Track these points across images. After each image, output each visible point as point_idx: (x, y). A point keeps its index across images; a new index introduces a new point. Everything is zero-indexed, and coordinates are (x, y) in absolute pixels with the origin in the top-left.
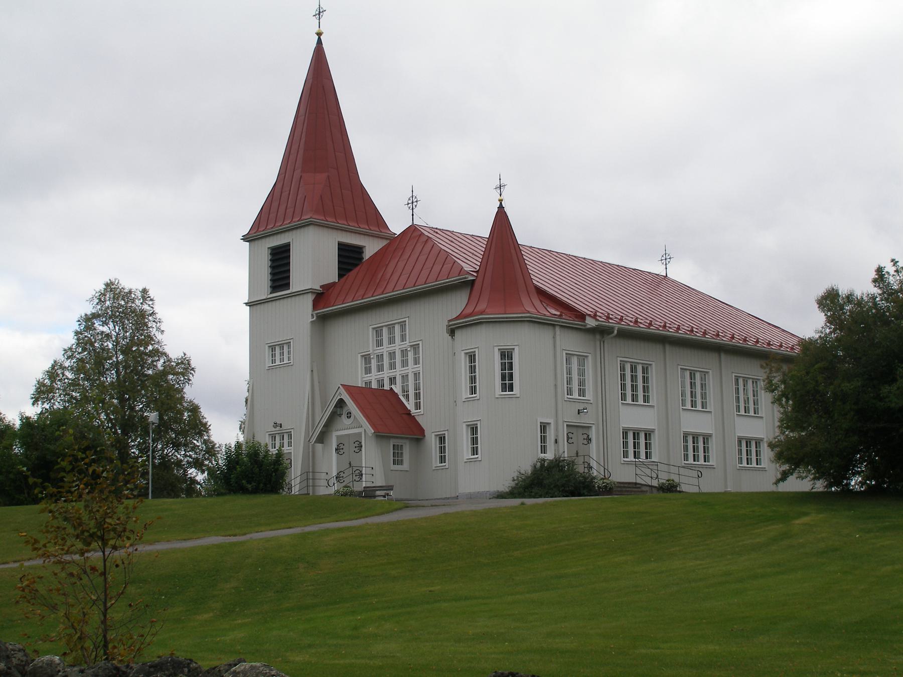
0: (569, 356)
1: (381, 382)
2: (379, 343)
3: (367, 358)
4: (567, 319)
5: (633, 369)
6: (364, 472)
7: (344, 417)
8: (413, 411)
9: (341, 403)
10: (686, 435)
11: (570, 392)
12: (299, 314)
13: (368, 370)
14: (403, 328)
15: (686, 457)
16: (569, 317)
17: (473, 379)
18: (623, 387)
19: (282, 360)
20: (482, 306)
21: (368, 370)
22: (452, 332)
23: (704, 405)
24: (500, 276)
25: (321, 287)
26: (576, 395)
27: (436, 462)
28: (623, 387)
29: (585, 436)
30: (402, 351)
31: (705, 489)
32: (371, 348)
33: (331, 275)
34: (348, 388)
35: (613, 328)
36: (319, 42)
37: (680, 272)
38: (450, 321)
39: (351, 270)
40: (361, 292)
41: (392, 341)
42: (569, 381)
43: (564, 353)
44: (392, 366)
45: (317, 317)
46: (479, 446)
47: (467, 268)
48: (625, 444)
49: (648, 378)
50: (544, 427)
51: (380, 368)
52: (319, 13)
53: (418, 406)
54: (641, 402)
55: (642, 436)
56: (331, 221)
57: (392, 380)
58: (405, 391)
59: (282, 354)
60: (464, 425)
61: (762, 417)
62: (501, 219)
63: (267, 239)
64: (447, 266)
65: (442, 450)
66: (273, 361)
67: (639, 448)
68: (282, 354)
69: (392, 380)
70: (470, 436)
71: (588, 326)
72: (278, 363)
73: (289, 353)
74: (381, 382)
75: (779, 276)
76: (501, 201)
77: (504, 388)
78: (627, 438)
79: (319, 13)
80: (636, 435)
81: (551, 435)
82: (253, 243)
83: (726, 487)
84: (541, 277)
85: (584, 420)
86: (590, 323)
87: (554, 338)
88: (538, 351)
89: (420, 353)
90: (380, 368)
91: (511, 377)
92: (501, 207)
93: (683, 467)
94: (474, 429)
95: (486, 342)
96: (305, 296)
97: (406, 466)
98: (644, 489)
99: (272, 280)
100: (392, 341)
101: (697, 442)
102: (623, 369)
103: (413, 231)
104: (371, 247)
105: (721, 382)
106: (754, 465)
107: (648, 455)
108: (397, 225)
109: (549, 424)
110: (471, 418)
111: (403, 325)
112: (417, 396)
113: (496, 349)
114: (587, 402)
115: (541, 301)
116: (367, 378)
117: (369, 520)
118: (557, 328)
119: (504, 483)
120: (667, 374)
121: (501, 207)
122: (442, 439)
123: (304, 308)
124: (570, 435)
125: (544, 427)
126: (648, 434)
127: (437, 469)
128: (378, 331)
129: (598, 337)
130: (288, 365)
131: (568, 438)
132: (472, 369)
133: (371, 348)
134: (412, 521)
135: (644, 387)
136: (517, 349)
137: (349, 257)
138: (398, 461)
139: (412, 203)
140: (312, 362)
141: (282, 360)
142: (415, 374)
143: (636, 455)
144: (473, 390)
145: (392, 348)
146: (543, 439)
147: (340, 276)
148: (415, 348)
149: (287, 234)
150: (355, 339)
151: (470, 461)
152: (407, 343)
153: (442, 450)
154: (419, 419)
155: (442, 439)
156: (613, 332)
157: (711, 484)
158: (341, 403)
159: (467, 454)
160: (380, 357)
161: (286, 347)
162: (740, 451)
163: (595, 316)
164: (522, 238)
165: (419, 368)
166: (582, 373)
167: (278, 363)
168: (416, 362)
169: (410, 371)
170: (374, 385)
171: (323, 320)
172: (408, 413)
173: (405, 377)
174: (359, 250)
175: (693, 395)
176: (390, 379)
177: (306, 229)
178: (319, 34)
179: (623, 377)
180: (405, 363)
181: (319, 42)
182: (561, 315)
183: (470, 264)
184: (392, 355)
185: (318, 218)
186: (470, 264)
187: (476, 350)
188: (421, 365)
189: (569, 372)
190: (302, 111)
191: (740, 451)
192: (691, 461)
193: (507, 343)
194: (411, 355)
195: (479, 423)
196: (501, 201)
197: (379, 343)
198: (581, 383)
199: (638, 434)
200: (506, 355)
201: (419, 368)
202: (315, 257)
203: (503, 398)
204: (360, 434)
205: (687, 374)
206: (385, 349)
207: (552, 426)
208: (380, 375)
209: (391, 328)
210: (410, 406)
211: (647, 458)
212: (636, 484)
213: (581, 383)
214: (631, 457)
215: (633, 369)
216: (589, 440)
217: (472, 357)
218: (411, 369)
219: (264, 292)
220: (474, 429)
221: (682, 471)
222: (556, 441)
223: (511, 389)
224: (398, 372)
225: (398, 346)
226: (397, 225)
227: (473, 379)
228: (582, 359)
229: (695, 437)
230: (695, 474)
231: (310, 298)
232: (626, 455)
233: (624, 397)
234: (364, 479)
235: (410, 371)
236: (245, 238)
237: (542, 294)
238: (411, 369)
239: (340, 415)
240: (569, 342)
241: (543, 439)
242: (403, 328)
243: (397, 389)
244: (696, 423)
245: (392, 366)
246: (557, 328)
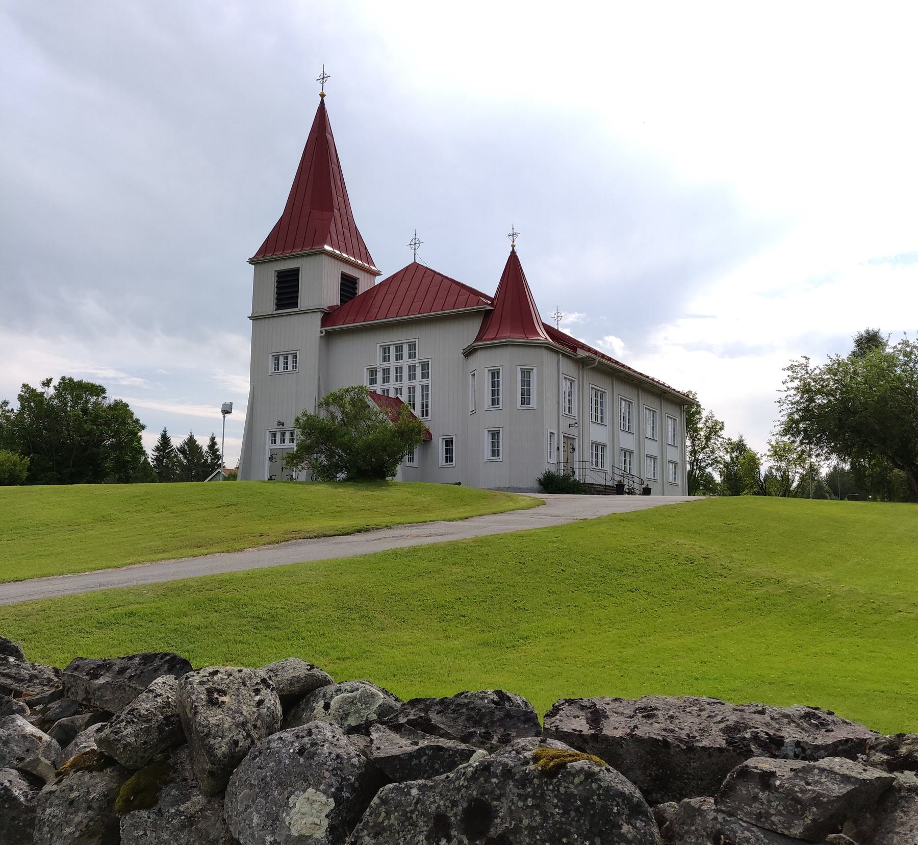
2: (386, 359)
12: (304, 332)
32: (379, 363)
36: (322, 103)
52: (323, 78)
53: (425, 413)
58: (412, 399)
60: (486, 431)
66: (277, 369)
69: (399, 391)
76: (513, 246)
79: (323, 78)
82: (259, 266)
86: (581, 353)
94: (495, 435)
97: (415, 463)
111: (412, 346)
112: (425, 406)
122: (449, 442)
126: (604, 447)
128: (386, 350)
133: (379, 363)
134: (519, 536)
136: (535, 369)
137: (348, 284)
139: (415, 244)
148: (425, 365)
160: (386, 371)
165: (428, 382)
171: (329, 337)
173: (412, 390)
178: (323, 96)
181: (322, 103)
184: (399, 370)
194: (418, 371)
197: (386, 359)
201: (428, 382)
206: (392, 364)
210: (417, 412)
216: (574, 449)
219: (269, 306)
220: (495, 435)
225: (405, 362)
231: (319, 316)
236: (252, 261)
238: (418, 382)
240: (566, 367)
243: (404, 398)
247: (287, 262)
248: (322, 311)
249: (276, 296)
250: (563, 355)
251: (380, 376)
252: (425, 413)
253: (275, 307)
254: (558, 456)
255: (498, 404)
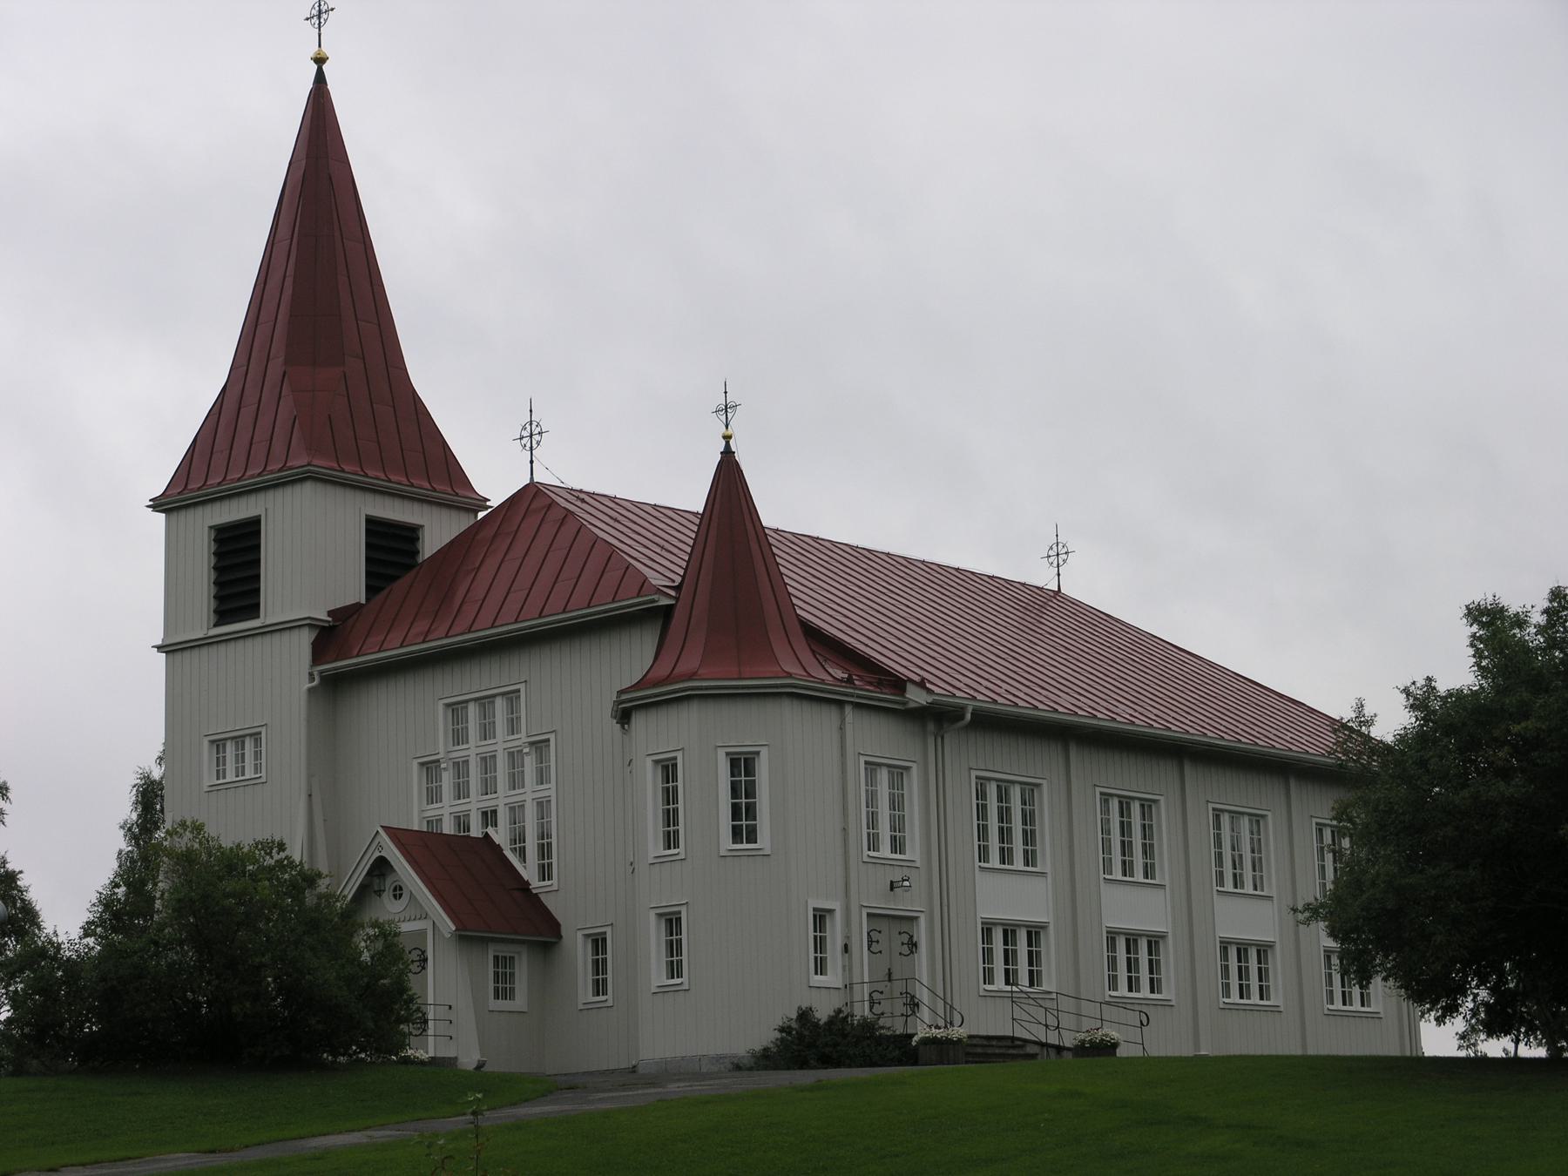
0: (872, 767)
1: (462, 821)
2: (459, 737)
3: (431, 768)
4: (864, 690)
5: (1003, 796)
6: (430, 1016)
7: (387, 897)
8: (535, 883)
9: (381, 867)
10: (1112, 936)
11: (873, 843)
12: (278, 672)
13: (433, 796)
14: (513, 706)
15: (1113, 983)
16: (868, 684)
17: (670, 817)
18: (983, 832)
19: (240, 771)
20: (690, 662)
21: (433, 796)
22: (624, 716)
23: (1148, 871)
24: (725, 601)
25: (330, 613)
26: (885, 851)
27: (586, 994)
28: (983, 832)
29: (905, 938)
30: (511, 754)
31: (1155, 1051)
33: (354, 591)
34: (400, 836)
35: (963, 708)
36: (320, 79)
37: (1090, 584)
38: (621, 692)
39: (394, 578)
40: (421, 626)
41: (487, 732)
42: (873, 821)
43: (862, 760)
44: (488, 787)
45: (322, 678)
46: (684, 958)
47: (656, 580)
48: (988, 955)
49: (1032, 813)
50: (821, 917)
51: (461, 791)
52: (319, 15)
53: (545, 872)
54: (1019, 864)
55: (1022, 937)
56: (350, 470)
57: (489, 817)
58: (518, 839)
59: (241, 758)
60: (652, 914)
61: (1270, 898)
62: (729, 478)
63: (208, 508)
64: (612, 577)
65: (599, 966)
66: (220, 774)
67: (1015, 963)
68: (241, 758)
69: (489, 817)
70: (663, 938)
71: (912, 705)
72: (230, 777)
73: (257, 755)
74: (462, 821)
75: (1366, 658)
77: (737, 834)
78: (990, 941)
80: (1009, 933)
81: (835, 935)
83: (1197, 1044)
84: (812, 601)
85: (901, 904)
86: (916, 697)
87: (842, 728)
88: (809, 756)
89: (547, 755)
90: (461, 791)
91: (751, 811)
92: (728, 454)
93: (1108, 1003)
94: (672, 922)
95: (698, 737)
96: (296, 632)
97: (520, 1002)
98: (1031, 1049)
99: (218, 598)
100: (487, 732)
101: (1137, 949)
102: (982, 794)
103: (532, 497)
104: (437, 531)
105: (1069, 782)
106: (1255, 999)
107: (1034, 979)
108: (494, 476)
109: (831, 911)
110: (668, 900)
111: (512, 696)
112: (544, 851)
113: (721, 753)
114: (910, 864)
115: (813, 652)
116: (432, 811)
117: (556, 1108)
118: (848, 709)
119: (763, 1035)
120: (1070, 798)
121: (728, 454)
122: (599, 943)
123: (292, 659)
124: (875, 936)
125: (821, 917)
127: (589, 1008)
128: (456, 709)
129: (931, 727)
130: (254, 783)
131: (870, 942)
132: (670, 796)
133: (441, 746)
135: (1025, 832)
136: (764, 752)
137: (389, 549)
138: (503, 993)
140: (310, 776)
141: (240, 771)
142: (540, 804)
143: (1010, 978)
144: (671, 840)
145: (487, 747)
146: (820, 944)
147: (371, 590)
148: (540, 746)
149: (252, 498)
150: (405, 726)
151: (663, 991)
152: (522, 737)
153: (599, 966)
154: (548, 901)
155: (599, 943)
156: (962, 717)
157: (1167, 1039)
158: (381, 867)
159: (658, 975)
160: (461, 767)
161: (249, 743)
162: (1113, 962)
163: (921, 684)
164: (772, 514)
165: (550, 790)
166: (896, 803)
167: (230, 777)
168: (542, 777)
169: (529, 797)
170: (448, 828)
172: (524, 886)
174: (410, 534)
175: (1126, 848)
176: (485, 814)
177: (297, 488)
179: (982, 811)
180: (516, 781)
181: (320, 79)
182: (850, 681)
183: (663, 571)
184: (488, 762)
185: (322, 464)
186: (663, 571)
187: (679, 755)
188: (553, 785)
189: (872, 799)
190: (284, 231)
191: (1113, 962)
192: (1123, 990)
193: (743, 742)
194: (530, 764)
195: (684, 910)
196: (727, 438)
197: (459, 737)
198: (897, 825)
199: (1014, 932)
200: (742, 765)
201: (550, 790)
202: (315, 548)
203: (735, 855)
204: (423, 933)
205: (1114, 805)
206: (473, 749)
207: (838, 915)
208: (461, 806)
209: (485, 702)
210: (528, 871)
211: (1031, 984)
212: (1013, 1039)
213: (897, 825)
214: (999, 984)
215: (1003, 796)
216: (913, 945)
217: (668, 770)
218: (530, 792)
219: (200, 624)
220: (672, 922)
221: (1109, 1012)
222: (846, 948)
223: (752, 838)
224: (502, 799)
225: (501, 742)
226: (494, 476)
227: (670, 817)
228: (898, 773)
229: (1132, 941)
230: (1134, 1018)
231: (305, 639)
232: (988, 977)
233: (984, 854)
234: (430, 1032)
235: (529, 797)
236: (158, 505)
237: (813, 635)
238: (530, 792)
239: (379, 893)
240: (874, 737)
241: (820, 944)
242: (513, 706)
243: (500, 836)
244: (1134, 908)
245: (488, 787)
246: (848, 709)
247: (407, 504)
248: (312, 624)
249: (213, 591)
250: (857, 706)
251: (447, 780)
252: (545, 872)
253: (213, 619)
254: (848, 969)
255: (676, 846)
